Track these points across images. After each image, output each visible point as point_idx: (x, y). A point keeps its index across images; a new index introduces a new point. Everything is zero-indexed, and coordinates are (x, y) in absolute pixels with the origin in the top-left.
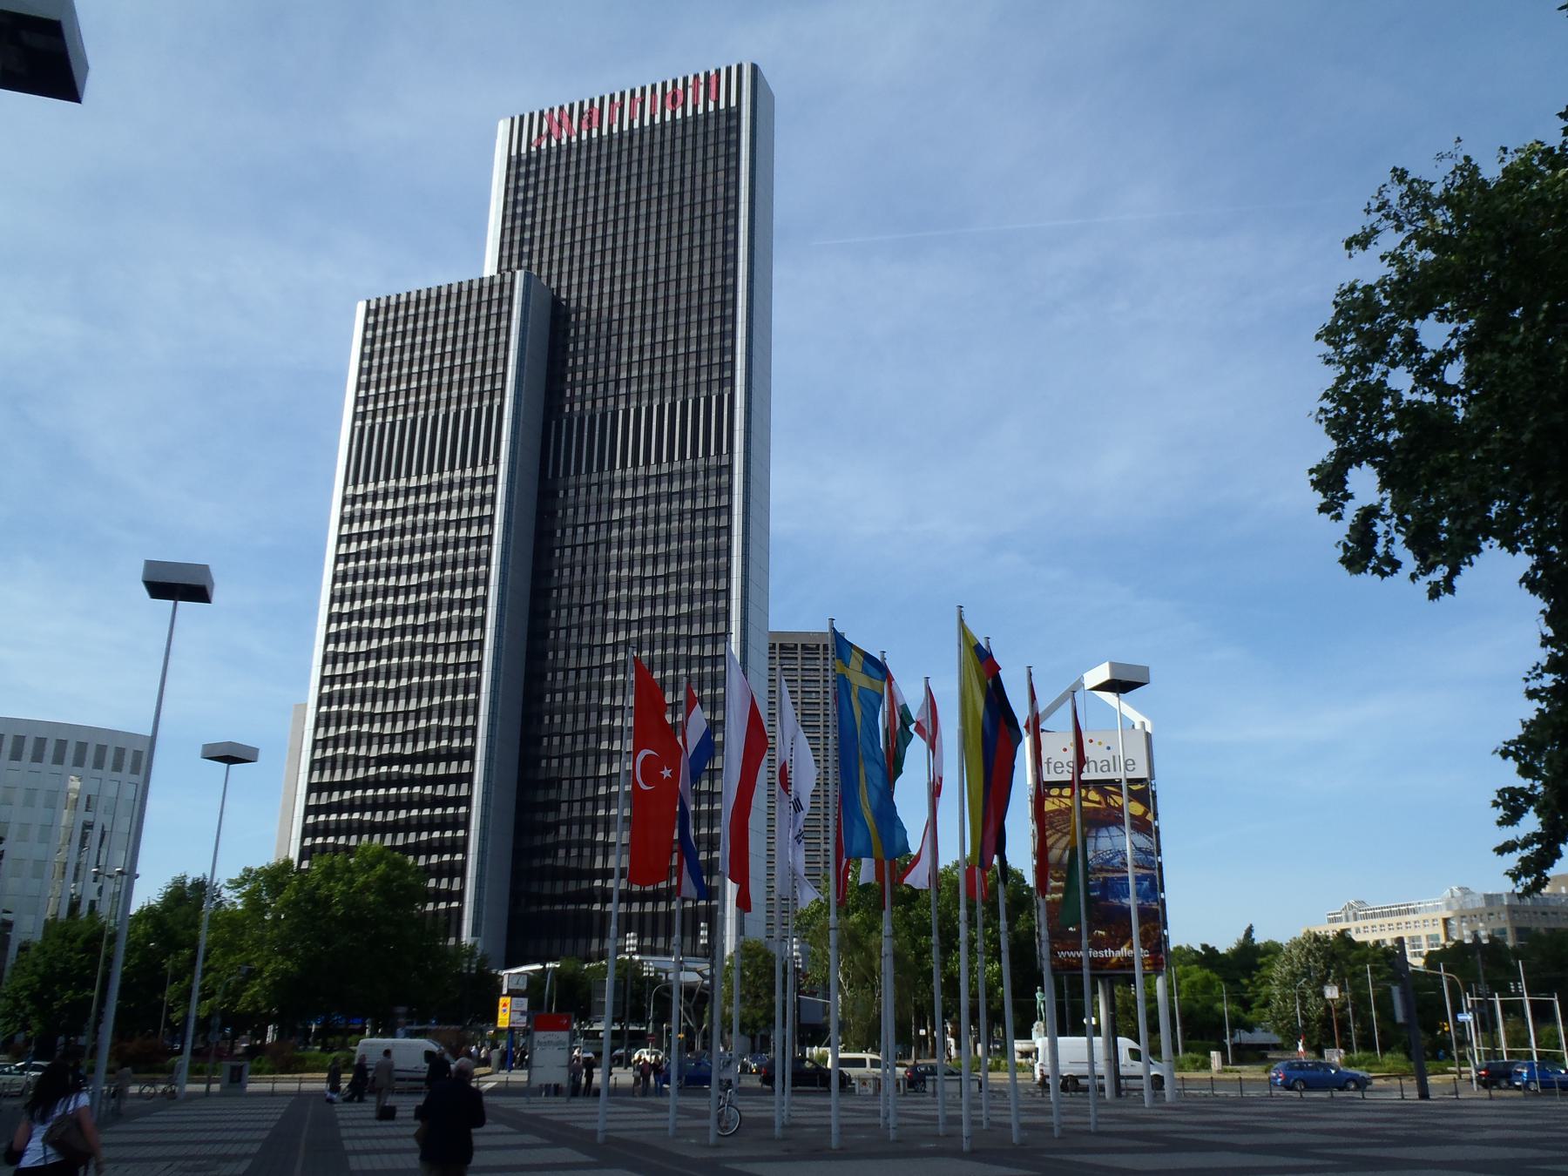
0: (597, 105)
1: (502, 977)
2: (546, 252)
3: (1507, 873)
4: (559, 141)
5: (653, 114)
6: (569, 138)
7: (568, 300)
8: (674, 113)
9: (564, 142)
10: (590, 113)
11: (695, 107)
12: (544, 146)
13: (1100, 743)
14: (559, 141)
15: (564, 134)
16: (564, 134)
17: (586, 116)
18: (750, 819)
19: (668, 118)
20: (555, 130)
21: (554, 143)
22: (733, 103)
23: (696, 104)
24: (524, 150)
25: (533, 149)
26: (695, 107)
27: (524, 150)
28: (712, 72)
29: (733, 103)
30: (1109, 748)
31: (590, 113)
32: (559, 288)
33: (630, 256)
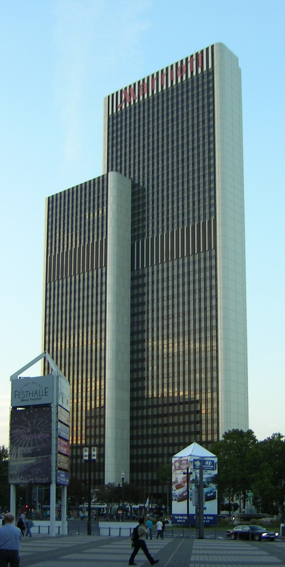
0: (146, 81)
1: (273, 517)
2: (185, 153)
3: (157, 561)
4: (130, 103)
5: (174, 80)
6: (134, 101)
7: (139, 183)
8: (182, 78)
9: (132, 103)
10: (143, 86)
11: (192, 72)
12: (123, 107)
13: (41, 387)
14: (130, 103)
15: (132, 99)
16: (132, 99)
17: (141, 87)
18: (31, 376)
19: (179, 81)
20: (128, 98)
21: (128, 105)
22: (210, 66)
23: (193, 71)
24: (115, 111)
25: (119, 110)
26: (192, 72)
27: (115, 111)
28: (199, 52)
29: (210, 66)
30: (25, 385)
31: (143, 86)
32: (134, 178)
33: (196, 160)
